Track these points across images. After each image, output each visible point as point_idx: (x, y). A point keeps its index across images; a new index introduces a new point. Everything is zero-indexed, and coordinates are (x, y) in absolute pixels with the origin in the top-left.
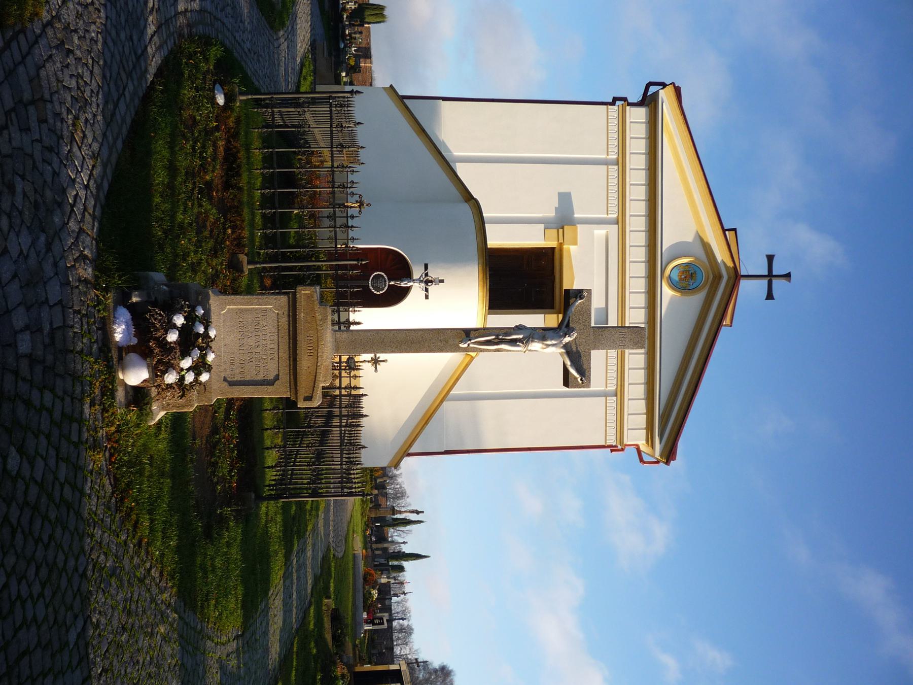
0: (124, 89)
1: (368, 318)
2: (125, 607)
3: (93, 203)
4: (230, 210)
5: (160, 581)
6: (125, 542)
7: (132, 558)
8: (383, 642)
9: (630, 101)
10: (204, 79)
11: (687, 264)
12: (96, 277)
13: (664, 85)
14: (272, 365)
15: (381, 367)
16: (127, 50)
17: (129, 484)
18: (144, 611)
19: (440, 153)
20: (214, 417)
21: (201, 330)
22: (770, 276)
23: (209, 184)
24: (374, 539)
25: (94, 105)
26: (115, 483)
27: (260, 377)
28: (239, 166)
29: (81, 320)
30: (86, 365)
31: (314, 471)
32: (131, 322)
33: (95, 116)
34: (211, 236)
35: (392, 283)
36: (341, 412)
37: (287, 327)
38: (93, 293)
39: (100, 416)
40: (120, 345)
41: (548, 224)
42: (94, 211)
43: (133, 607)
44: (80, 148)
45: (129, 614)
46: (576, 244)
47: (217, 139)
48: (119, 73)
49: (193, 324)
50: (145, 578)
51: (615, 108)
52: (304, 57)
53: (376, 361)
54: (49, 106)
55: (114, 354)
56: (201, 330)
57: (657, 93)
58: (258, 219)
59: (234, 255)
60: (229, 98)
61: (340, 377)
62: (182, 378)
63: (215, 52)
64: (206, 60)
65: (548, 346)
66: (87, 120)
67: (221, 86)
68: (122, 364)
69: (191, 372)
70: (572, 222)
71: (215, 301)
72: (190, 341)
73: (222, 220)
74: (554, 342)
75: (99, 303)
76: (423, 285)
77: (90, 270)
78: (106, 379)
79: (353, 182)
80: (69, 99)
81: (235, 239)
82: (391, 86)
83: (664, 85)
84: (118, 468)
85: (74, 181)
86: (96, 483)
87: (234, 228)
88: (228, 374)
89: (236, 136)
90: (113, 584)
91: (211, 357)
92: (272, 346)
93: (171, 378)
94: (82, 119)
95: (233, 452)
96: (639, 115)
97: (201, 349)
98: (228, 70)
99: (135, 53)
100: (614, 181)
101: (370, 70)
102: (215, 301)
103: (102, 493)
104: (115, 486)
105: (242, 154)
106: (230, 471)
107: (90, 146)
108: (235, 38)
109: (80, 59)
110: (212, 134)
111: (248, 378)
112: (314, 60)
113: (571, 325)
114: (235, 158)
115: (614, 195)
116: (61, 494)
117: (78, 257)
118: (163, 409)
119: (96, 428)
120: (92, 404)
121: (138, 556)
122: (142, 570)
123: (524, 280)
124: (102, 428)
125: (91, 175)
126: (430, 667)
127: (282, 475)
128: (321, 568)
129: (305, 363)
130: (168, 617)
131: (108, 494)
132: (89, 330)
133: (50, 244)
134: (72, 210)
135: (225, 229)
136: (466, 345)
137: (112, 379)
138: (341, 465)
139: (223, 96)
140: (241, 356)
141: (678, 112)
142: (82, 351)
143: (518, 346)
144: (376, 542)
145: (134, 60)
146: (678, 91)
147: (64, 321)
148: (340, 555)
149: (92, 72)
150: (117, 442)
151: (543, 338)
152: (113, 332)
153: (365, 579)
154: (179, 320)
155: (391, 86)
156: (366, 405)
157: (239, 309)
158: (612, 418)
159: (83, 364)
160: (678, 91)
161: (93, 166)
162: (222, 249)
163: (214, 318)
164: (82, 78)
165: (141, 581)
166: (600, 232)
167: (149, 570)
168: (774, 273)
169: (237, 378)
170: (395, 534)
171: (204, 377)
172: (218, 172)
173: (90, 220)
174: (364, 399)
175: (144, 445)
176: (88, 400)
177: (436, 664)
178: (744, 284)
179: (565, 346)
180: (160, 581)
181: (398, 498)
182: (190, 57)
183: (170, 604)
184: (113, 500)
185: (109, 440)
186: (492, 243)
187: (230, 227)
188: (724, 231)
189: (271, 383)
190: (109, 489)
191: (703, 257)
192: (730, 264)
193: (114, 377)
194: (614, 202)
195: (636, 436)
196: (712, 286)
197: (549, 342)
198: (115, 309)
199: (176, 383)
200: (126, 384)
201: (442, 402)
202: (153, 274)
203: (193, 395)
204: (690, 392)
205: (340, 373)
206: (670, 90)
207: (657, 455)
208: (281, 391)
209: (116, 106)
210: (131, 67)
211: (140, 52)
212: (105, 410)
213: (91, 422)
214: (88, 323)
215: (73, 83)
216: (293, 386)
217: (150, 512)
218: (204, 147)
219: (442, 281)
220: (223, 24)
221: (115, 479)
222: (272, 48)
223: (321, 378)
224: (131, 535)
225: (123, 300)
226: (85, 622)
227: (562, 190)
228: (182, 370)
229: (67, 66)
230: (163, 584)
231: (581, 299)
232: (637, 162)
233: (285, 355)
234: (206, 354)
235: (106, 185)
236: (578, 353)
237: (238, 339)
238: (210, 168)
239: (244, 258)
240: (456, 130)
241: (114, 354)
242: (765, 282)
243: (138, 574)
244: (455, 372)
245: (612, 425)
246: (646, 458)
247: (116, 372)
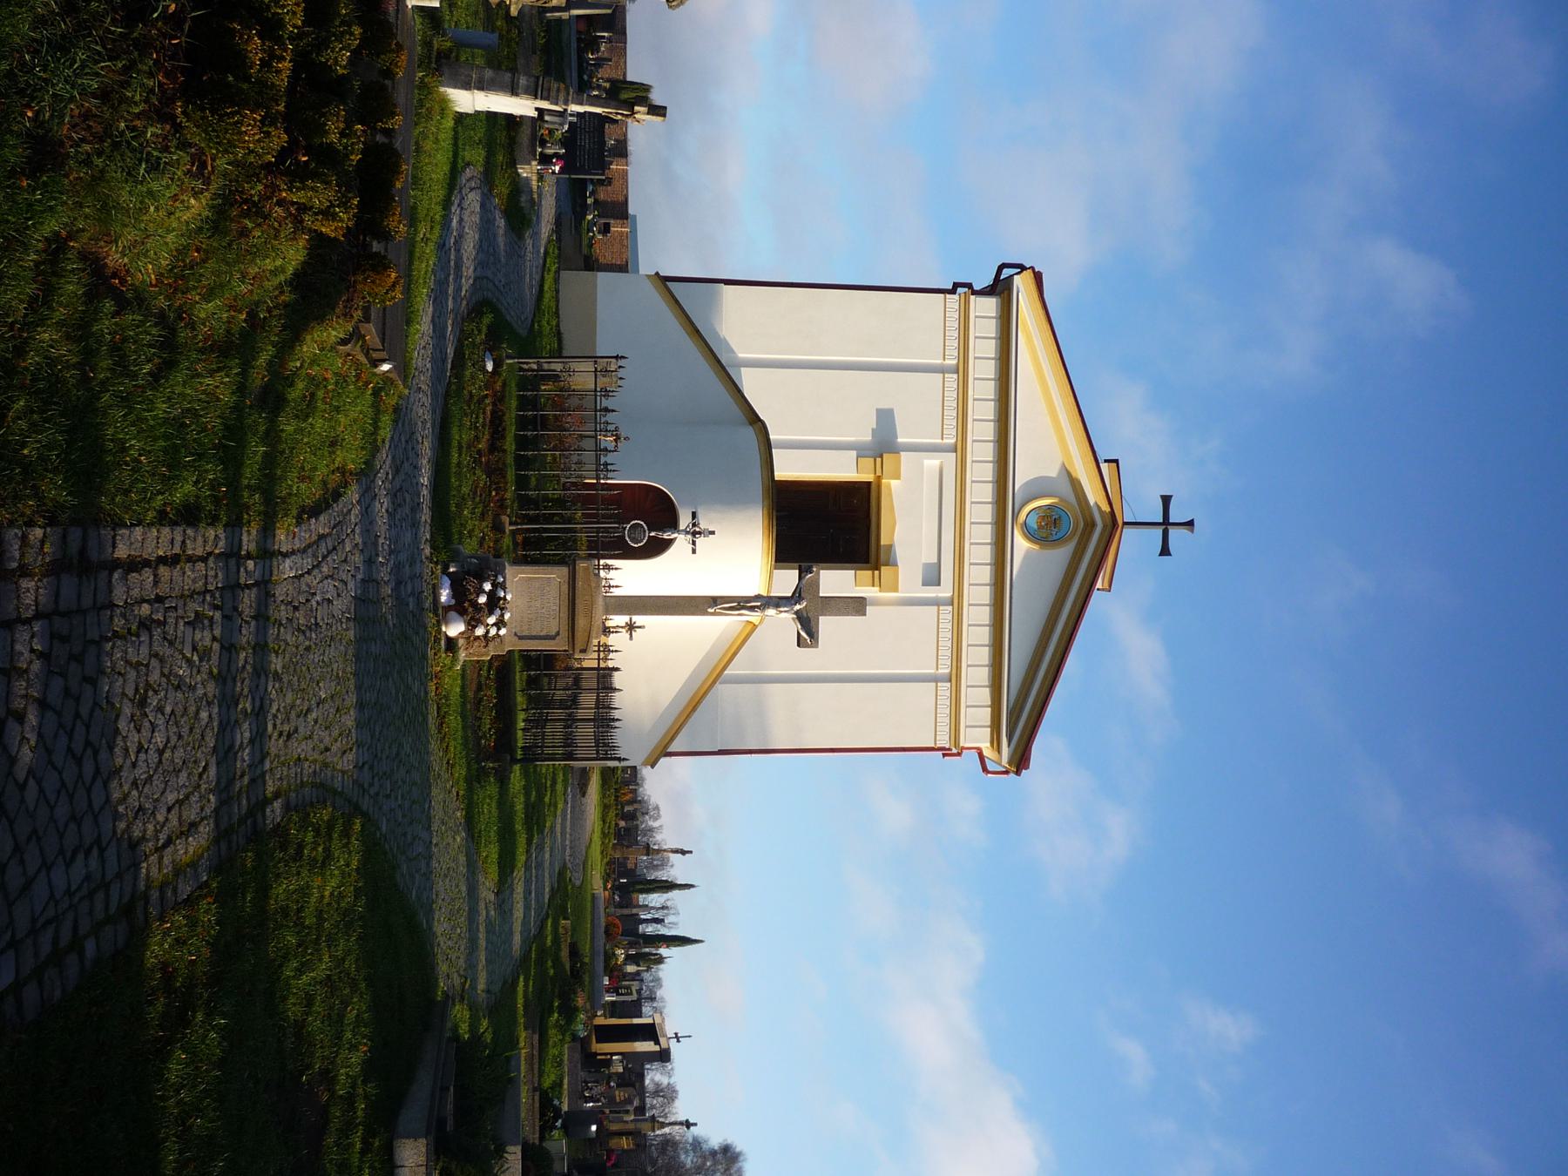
1: (629, 576)
8: (625, 1046)
9: (976, 288)
11: (1049, 507)
13: (1022, 268)
15: (637, 634)
19: (719, 361)
20: (479, 675)
22: (1166, 523)
41: (862, 451)
46: (898, 477)
51: (956, 297)
53: (631, 627)
59: (497, 516)
60: (497, 365)
71: (510, 570)
72: (494, 603)
76: (689, 537)
91: (507, 616)
93: (480, 631)
96: (986, 307)
100: (952, 395)
101: (624, 175)
102: (510, 570)
112: (559, 240)
115: (951, 414)
123: (826, 527)
126: (704, 1146)
129: (581, 622)
141: (1039, 305)
146: (1038, 278)
147: (64, 537)
148: (578, 883)
151: (777, 606)
153: (607, 932)
154: (487, 587)
160: (1038, 278)
166: (932, 463)
171: (503, 632)
177: (715, 1142)
179: (797, 613)
186: (781, 474)
189: (553, 638)
191: (1072, 499)
192: (1107, 509)
194: (951, 422)
195: (977, 735)
196: (1082, 537)
201: (714, 682)
204: (1050, 677)
206: (1028, 274)
219: (713, 533)
227: (881, 406)
232: (983, 369)
233: (564, 615)
237: (526, 600)
239: (505, 519)
240: (742, 324)
242: (1159, 531)
246: (990, 766)
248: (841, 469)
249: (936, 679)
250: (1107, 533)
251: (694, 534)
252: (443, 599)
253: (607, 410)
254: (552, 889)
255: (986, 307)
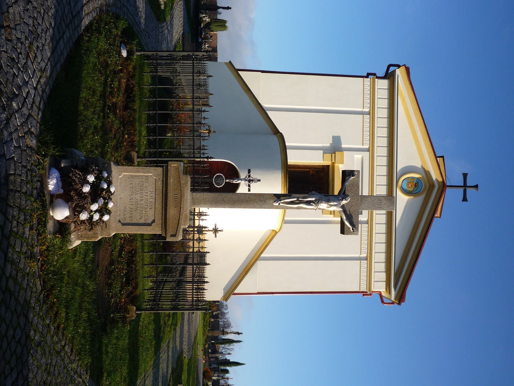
0: (63, 34)
2: (46, 369)
3: (39, 99)
4: (128, 124)
5: (71, 355)
6: (49, 325)
7: (53, 336)
10: (114, 39)
12: (39, 147)
14: (151, 212)
15: (219, 234)
16: (67, 12)
17: (53, 287)
18: (59, 374)
20: (111, 255)
21: (105, 186)
22: (465, 186)
23: (115, 105)
24: (210, 351)
25: (43, 39)
26: (44, 285)
27: (142, 221)
28: (134, 96)
29: (27, 172)
30: (29, 202)
31: (175, 293)
32: (59, 179)
33: (43, 45)
34: (115, 138)
35: (227, 181)
36: (193, 286)
37: (161, 188)
38: (35, 157)
39: (36, 238)
40: (52, 193)
42: (40, 104)
43: (52, 369)
44: (32, 63)
45: (49, 373)
46: (342, 163)
47: (121, 78)
48: (60, 23)
49: (100, 183)
50: (61, 351)
51: (369, 79)
52: (178, 42)
54: (14, 32)
55: (47, 198)
56: (105, 186)
57: (395, 71)
58: (144, 117)
60: (130, 53)
61: (194, 220)
62: (91, 217)
63: (122, 24)
64: (117, 28)
65: (331, 206)
66: (38, 47)
67: (125, 45)
68: (52, 205)
69: (97, 213)
70: (341, 150)
71: (115, 169)
73: (122, 129)
74: (335, 203)
75: (39, 164)
77: (34, 141)
78: (41, 214)
79: (204, 146)
80: (28, 30)
81: (130, 142)
82: (230, 62)
83: (399, 66)
84: (46, 275)
85: (27, 82)
86: (31, 282)
87: (130, 134)
88: (121, 218)
89: (133, 77)
90: (39, 351)
91: (111, 205)
92: (151, 200)
93: (84, 216)
94: (35, 44)
95: (123, 279)
96: (384, 84)
97: (104, 199)
98: (129, 36)
99: (72, 14)
100: (367, 125)
103: (34, 289)
104: (44, 287)
105: (136, 88)
106: (121, 291)
107: (39, 63)
108: (135, 20)
109: (36, 8)
110: (118, 74)
111: (135, 221)
113: (346, 193)
114: (132, 90)
116: (7, 285)
117: (27, 132)
118: (78, 239)
119: (33, 245)
120: (31, 229)
121: (57, 336)
122: (59, 346)
124: (37, 246)
125: (39, 82)
127: (155, 294)
128: (177, 364)
129: (172, 212)
130: (75, 380)
131: (39, 291)
132: (32, 180)
133: (9, 119)
134: (25, 101)
135: (124, 135)
136: (277, 204)
137: (45, 214)
138: (193, 290)
139: (126, 51)
140: (130, 206)
141: (408, 83)
142: (26, 192)
143: (312, 205)
144: (212, 353)
145: (71, 18)
149: (43, 18)
150: (46, 257)
152: (47, 184)
155: (230, 62)
156: (208, 259)
157: (131, 175)
158: (364, 274)
159: (26, 201)
160: (408, 70)
161: (41, 77)
162: (121, 147)
163: (114, 180)
164: (36, 20)
165: (58, 353)
167: (64, 347)
168: (468, 185)
169: (128, 221)
170: (221, 348)
171: (106, 218)
172: (121, 98)
173: (37, 110)
174: (208, 255)
175: (64, 262)
176: (28, 225)
178: (448, 190)
179: (343, 207)
180: (71, 355)
181: (226, 328)
182: (106, 24)
183: (76, 372)
184: (42, 296)
185: (41, 255)
187: (127, 134)
188: (436, 157)
189: (150, 225)
190: (39, 288)
193: (47, 213)
194: (367, 138)
195: (379, 286)
196: (429, 193)
197: (332, 203)
198: (50, 169)
199: (87, 220)
200: (55, 219)
202: (77, 152)
203: (98, 229)
205: (194, 218)
206: (403, 69)
207: (393, 298)
208: (156, 230)
209: (58, 43)
210: (69, 21)
211: (75, 13)
212: (39, 234)
213: (30, 240)
214: (31, 175)
215: (30, 22)
216: (164, 227)
217: (67, 307)
218: (112, 81)
220: (128, 9)
221: (44, 282)
222: (157, 31)
223: (182, 222)
224: (53, 320)
225: (55, 164)
226: (18, 375)
228: (92, 211)
229: (27, 10)
230: (72, 357)
231: (353, 176)
233: (159, 206)
234: (107, 203)
235: (47, 90)
236: (351, 215)
238: (116, 95)
241: (47, 198)
242: (462, 190)
243: (56, 348)
244: (265, 242)
245: (364, 278)
246: (385, 300)
247: (48, 210)
248: (316, 159)
249: (360, 259)
250: (440, 190)
251: (250, 181)
252: (51, 187)
253: (205, 118)
254: (173, 369)
255: (384, 84)
